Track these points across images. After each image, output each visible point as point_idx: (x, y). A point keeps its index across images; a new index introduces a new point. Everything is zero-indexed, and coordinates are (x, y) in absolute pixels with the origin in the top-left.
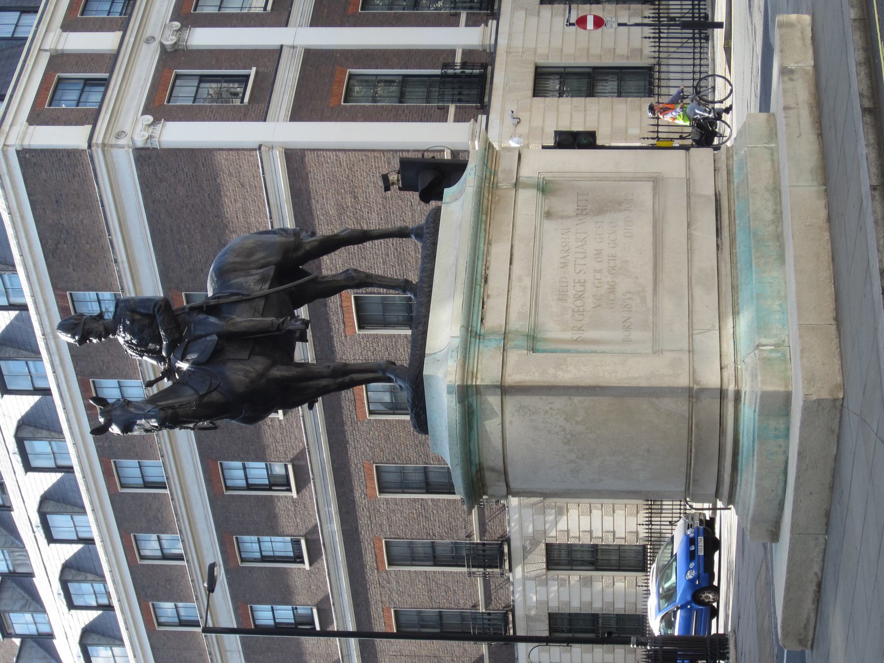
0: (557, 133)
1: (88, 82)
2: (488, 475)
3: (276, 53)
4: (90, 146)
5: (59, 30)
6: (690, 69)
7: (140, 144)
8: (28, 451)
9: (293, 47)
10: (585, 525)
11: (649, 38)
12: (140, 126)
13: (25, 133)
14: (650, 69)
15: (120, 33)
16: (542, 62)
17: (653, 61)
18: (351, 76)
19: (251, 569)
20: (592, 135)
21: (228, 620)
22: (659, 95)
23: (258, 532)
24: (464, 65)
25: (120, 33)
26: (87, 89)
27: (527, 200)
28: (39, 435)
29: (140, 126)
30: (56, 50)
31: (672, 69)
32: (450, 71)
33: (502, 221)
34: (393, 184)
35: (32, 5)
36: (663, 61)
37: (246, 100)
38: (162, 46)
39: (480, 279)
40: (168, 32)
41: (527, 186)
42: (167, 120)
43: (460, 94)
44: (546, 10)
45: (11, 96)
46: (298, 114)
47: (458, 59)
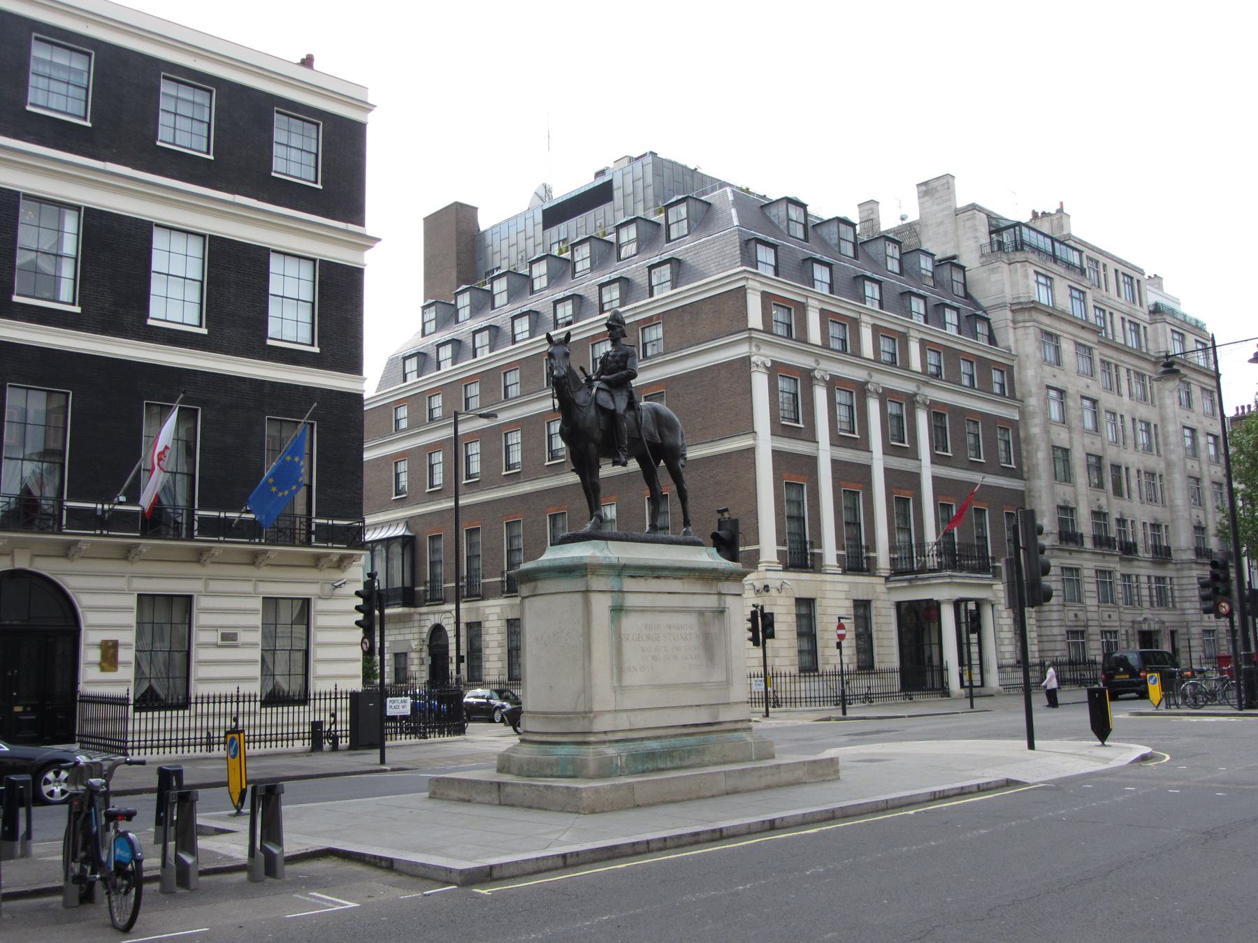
0: (772, 614)
1: (789, 326)
2: (533, 584)
3: (813, 440)
4: (750, 329)
5: (820, 307)
6: (821, 695)
7: (753, 359)
8: (613, 286)
9: (818, 450)
10: (492, 644)
11: (238, 692)
12: (763, 359)
13: (756, 290)
14: (872, 667)
15: (820, 344)
16: (818, 603)
17: (820, 672)
18: (802, 485)
19: (501, 439)
20: (772, 636)
21: (462, 429)
22: (800, 676)
23: (482, 454)
24: (813, 554)
25: (820, 344)
26: (785, 326)
27: (711, 602)
28: (180, 430)
29: (763, 359)
30: (808, 306)
31: (821, 683)
32: (808, 546)
33: (698, 587)
34: (722, 515)
35: (835, 290)
36: (821, 678)
37: (783, 422)
38: (814, 370)
39: (656, 574)
40: (822, 373)
41: (719, 600)
42: (769, 375)
43: (795, 553)
44: (850, 604)
45: (778, 281)
46: (776, 454)
47: (816, 551)
